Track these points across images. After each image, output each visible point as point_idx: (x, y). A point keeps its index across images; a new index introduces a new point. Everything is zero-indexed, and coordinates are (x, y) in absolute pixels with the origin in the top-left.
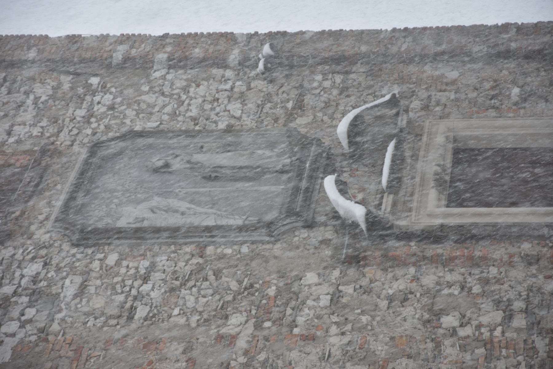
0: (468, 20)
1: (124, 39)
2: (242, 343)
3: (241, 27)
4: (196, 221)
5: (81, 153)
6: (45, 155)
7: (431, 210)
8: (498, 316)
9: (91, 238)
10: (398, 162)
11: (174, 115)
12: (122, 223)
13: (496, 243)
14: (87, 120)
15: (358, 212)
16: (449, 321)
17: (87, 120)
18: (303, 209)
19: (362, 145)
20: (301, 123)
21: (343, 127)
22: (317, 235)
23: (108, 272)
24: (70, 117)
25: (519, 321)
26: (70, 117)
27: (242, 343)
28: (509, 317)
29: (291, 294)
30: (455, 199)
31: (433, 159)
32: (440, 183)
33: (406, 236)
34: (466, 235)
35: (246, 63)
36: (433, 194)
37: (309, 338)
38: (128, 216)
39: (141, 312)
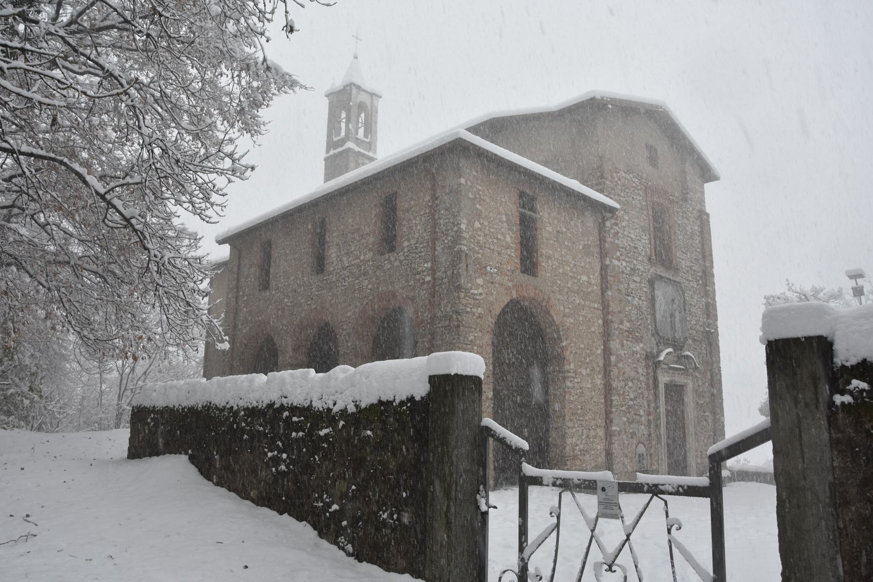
0: (724, 388)
1: (714, 290)
2: (621, 326)
3: (719, 323)
4: (658, 312)
5: (678, 279)
6: (677, 270)
7: (664, 379)
8: (632, 397)
9: (651, 283)
10: (677, 369)
11: (691, 305)
12: (656, 292)
13: (846, 568)
14: (688, 280)
15: (662, 358)
16: (630, 384)
17: (688, 280)
18: (663, 342)
19: (681, 358)
20: (690, 341)
21: (688, 353)
22: (656, 348)
23: (641, 289)
24: (837, 552)
25: (631, 403)
26: (837, 552)
27: (621, 326)
28: (632, 400)
29: (638, 340)
30: (667, 386)
31: (680, 379)
32: (672, 381)
33: (655, 372)
34: (656, 386)
35: (709, 325)
36: (668, 379)
37: (623, 345)
38: (658, 293)
39: (630, 298)
